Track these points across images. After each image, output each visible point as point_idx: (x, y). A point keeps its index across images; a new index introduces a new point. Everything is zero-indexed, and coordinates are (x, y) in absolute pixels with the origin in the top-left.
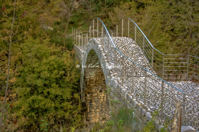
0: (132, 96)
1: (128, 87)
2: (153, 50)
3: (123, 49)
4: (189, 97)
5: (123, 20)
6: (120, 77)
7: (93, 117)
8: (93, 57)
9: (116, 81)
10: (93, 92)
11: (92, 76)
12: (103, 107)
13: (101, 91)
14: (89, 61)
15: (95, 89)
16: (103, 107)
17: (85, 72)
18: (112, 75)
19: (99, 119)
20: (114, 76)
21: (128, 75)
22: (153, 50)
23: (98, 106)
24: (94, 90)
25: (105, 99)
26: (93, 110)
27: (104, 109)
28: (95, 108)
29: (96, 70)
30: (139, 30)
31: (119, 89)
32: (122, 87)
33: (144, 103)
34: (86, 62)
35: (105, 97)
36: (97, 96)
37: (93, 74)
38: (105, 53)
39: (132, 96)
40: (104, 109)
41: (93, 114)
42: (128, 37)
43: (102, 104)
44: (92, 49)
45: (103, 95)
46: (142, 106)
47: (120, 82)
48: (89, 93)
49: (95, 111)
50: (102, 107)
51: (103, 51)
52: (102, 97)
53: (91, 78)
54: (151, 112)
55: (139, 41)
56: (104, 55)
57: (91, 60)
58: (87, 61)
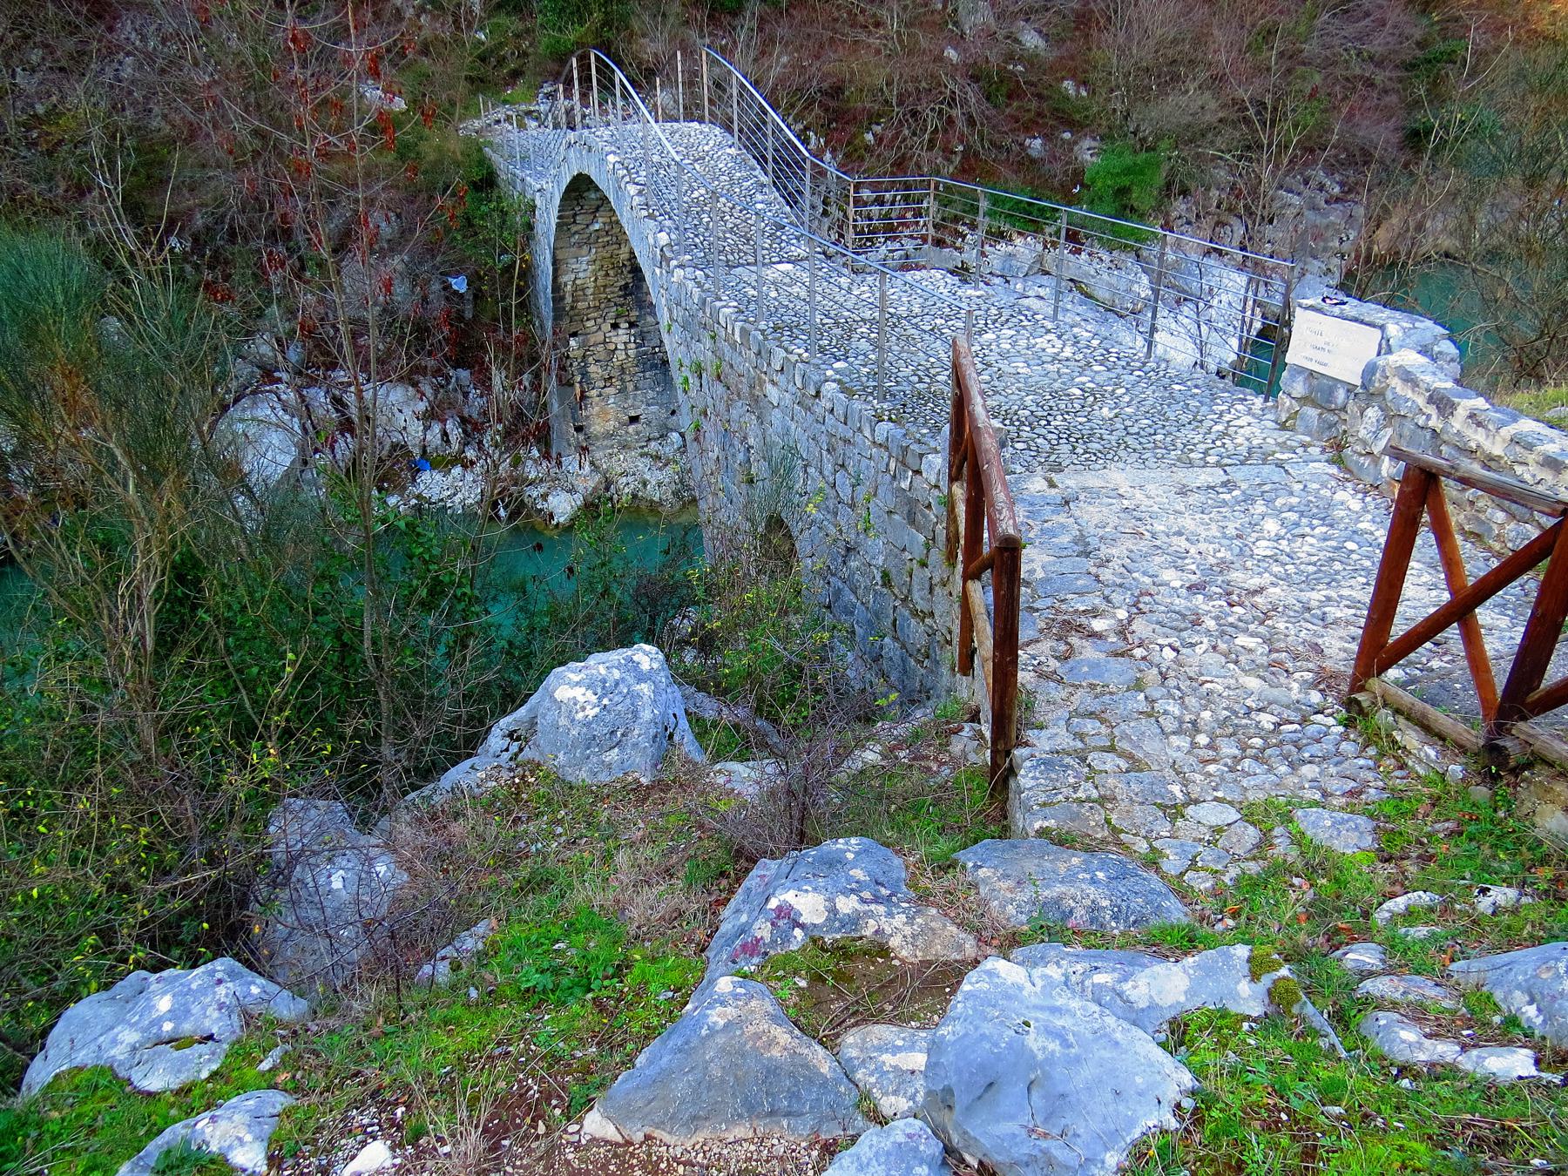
0: (763, 332)
1: (740, 302)
2: (808, 166)
3: (697, 167)
4: (950, 323)
5: (679, 58)
6: (702, 270)
7: (598, 415)
8: (582, 202)
9: (691, 284)
10: (588, 331)
11: (581, 275)
12: (628, 378)
13: (615, 326)
14: (568, 217)
15: (595, 319)
16: (628, 378)
17: (555, 262)
18: (674, 263)
19: (617, 419)
20: (681, 266)
21: (728, 261)
22: (808, 166)
23: (611, 378)
24: (592, 322)
25: (630, 352)
26: (594, 393)
27: (630, 386)
28: (602, 384)
29: (594, 251)
30: (607, 66)
31: (708, 311)
32: (718, 304)
33: (806, 351)
34: (558, 224)
35: (633, 346)
36: (605, 342)
37: (584, 266)
38: (637, 184)
39: (763, 332)
40: (630, 386)
41: (597, 404)
42: (707, 120)
43: (623, 370)
44: (580, 175)
45: (625, 338)
46: (802, 362)
47: (707, 286)
48: (574, 335)
49: (600, 395)
50: (622, 380)
51: (627, 179)
52: (621, 346)
53: (578, 282)
54: (839, 382)
55: (752, 138)
56: (632, 193)
57: (575, 215)
58: (559, 218)
